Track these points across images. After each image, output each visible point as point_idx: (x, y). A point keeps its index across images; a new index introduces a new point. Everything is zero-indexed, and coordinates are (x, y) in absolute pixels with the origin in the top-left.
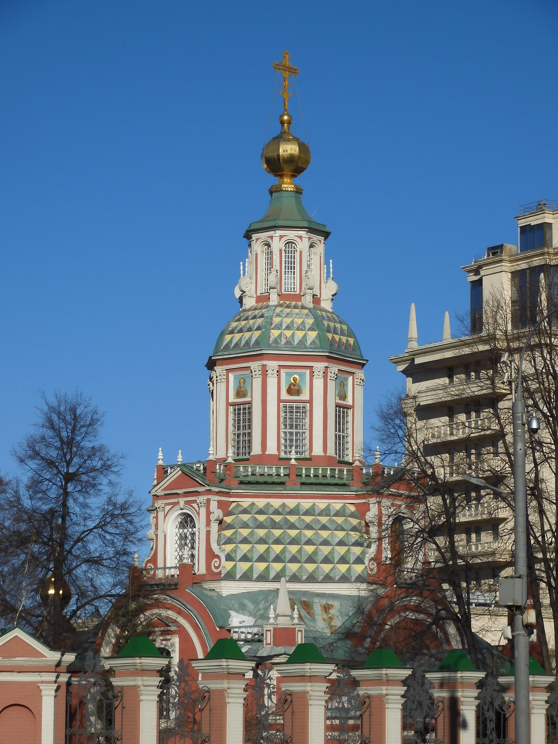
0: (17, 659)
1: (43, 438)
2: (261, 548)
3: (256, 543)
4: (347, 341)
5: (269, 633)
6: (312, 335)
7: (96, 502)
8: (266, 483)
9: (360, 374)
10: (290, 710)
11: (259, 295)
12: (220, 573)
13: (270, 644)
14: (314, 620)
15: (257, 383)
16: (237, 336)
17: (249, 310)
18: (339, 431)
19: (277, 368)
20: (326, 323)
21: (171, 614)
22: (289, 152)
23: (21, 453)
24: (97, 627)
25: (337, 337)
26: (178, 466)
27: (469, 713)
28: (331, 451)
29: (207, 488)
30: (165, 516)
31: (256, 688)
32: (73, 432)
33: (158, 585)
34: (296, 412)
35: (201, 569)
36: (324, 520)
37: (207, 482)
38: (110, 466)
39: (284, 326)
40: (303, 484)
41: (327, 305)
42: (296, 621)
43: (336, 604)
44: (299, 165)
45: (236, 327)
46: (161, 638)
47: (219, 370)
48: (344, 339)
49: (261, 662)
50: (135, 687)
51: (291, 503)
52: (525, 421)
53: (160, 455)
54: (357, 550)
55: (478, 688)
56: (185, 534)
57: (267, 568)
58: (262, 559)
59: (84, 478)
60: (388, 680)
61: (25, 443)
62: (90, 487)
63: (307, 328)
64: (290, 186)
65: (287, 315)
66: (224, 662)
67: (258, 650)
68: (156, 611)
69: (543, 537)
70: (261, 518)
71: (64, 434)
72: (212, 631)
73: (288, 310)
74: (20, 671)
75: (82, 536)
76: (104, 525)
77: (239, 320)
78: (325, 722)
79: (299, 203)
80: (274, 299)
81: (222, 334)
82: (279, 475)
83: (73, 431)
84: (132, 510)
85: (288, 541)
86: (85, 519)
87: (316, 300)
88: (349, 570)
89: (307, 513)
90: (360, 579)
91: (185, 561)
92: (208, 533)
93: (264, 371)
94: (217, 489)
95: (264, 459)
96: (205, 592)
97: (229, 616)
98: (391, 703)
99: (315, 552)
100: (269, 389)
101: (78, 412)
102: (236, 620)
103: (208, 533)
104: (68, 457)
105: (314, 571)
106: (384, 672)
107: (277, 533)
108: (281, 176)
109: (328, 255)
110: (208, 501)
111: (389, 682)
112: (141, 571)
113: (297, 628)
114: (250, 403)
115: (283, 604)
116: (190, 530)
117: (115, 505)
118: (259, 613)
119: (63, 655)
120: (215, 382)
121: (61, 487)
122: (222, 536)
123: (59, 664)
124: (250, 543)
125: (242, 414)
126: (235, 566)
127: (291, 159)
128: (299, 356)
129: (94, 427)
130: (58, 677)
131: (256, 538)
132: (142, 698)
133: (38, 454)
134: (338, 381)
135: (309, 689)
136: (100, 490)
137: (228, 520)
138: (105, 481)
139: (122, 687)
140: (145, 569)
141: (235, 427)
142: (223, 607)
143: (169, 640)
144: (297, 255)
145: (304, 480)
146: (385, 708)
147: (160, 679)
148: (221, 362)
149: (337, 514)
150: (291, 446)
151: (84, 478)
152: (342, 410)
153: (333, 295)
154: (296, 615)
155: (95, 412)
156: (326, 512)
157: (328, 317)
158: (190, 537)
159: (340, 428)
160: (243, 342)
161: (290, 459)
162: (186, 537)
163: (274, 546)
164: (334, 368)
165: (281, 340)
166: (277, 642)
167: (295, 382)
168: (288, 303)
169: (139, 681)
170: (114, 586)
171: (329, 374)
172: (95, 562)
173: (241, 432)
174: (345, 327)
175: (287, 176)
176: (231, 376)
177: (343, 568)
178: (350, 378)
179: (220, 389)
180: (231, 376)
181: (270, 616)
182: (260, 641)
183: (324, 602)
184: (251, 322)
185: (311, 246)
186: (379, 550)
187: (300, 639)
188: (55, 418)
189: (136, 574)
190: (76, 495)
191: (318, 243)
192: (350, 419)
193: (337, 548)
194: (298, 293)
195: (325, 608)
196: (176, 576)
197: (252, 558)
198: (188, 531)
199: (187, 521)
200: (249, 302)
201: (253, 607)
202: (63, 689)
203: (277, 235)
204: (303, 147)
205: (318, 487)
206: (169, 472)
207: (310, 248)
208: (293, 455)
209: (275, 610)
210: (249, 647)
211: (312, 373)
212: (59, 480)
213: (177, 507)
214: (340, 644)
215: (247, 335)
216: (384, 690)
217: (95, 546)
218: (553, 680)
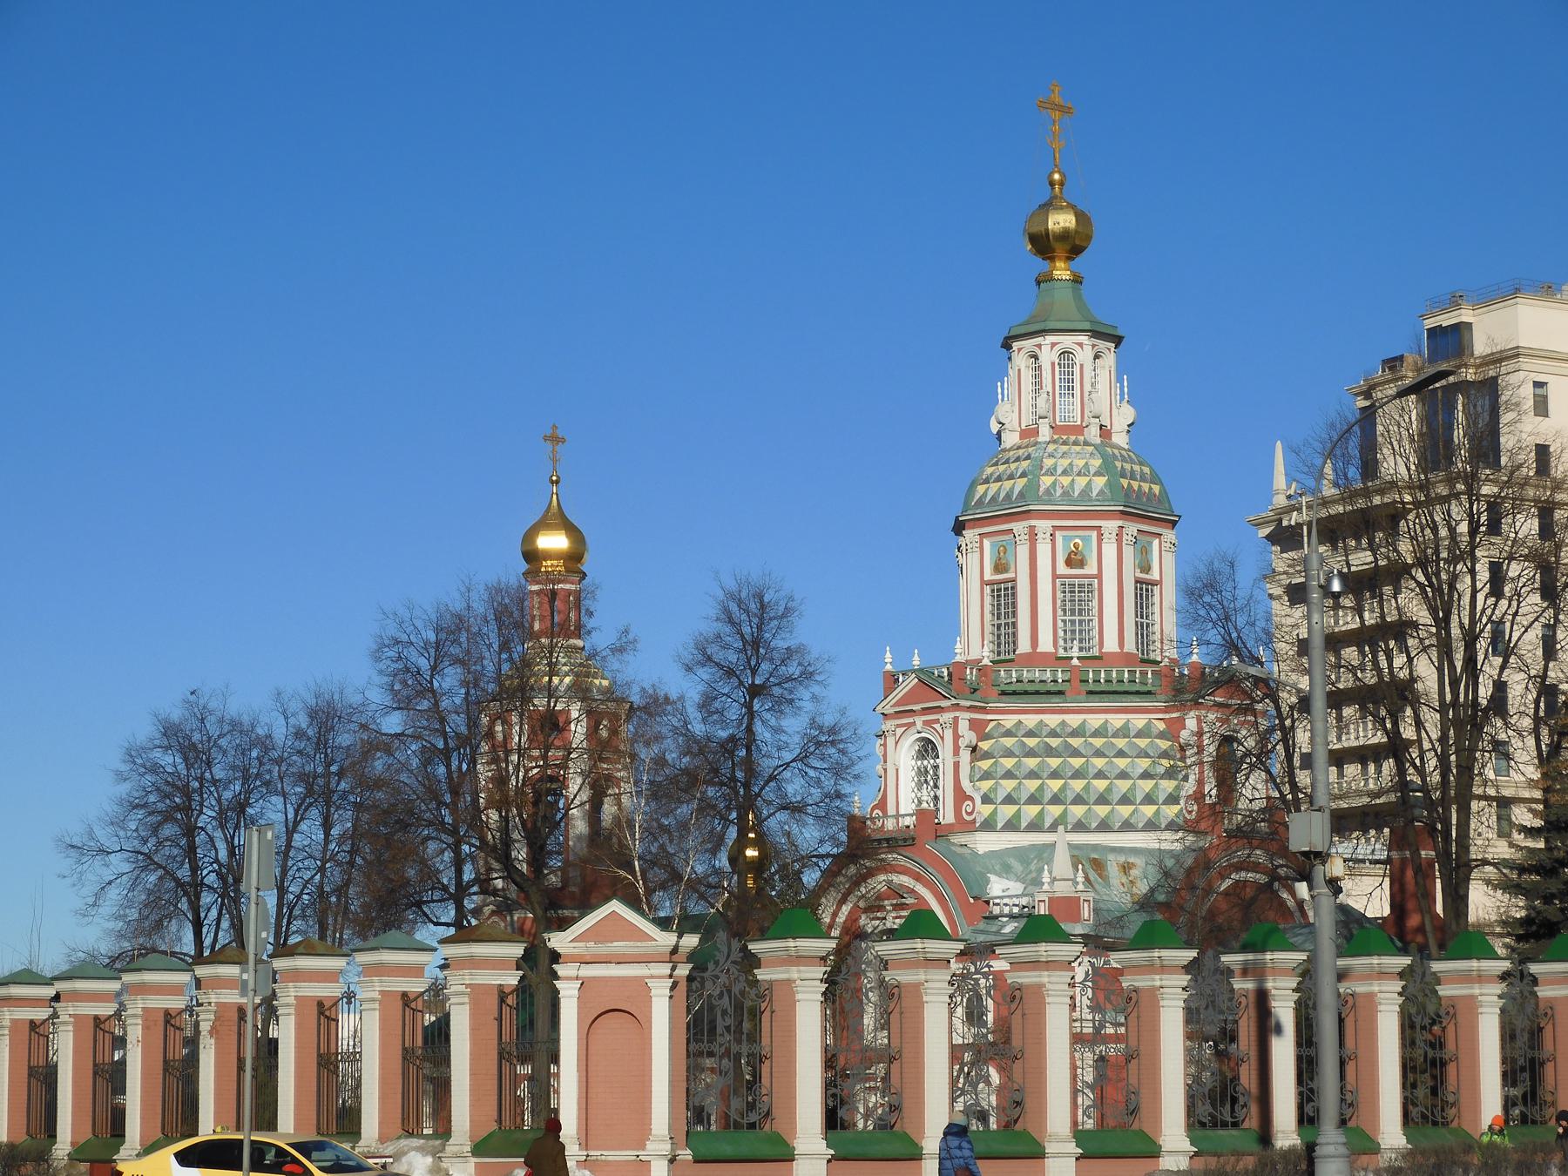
2: (1032, 785)
6: (1100, 482)
7: (794, 726)
8: (1037, 693)
9: (1169, 535)
10: (1019, 1012)
14: (1107, 884)
15: (1023, 552)
16: (994, 487)
19: (1050, 531)
20: (1119, 464)
21: (905, 880)
23: (688, 658)
25: (1135, 485)
26: (914, 671)
27: (1284, 1011)
28: (1130, 646)
29: (954, 701)
32: (759, 628)
33: (887, 840)
35: (947, 816)
36: (1121, 743)
38: (811, 674)
39: (1059, 471)
40: (1090, 693)
41: (1120, 439)
42: (1081, 887)
43: (1139, 861)
48: (1145, 487)
50: (789, 982)
51: (1074, 720)
53: (888, 657)
54: (1168, 786)
55: (1187, 973)
58: (1033, 800)
59: (777, 691)
62: (783, 704)
65: (1064, 455)
66: (918, 944)
68: (882, 877)
69: (1422, 759)
70: (1031, 742)
71: (746, 630)
73: (1065, 448)
74: (621, 961)
77: (996, 464)
79: (1078, 297)
80: (1045, 433)
83: (759, 628)
84: (844, 735)
86: (779, 749)
87: (1105, 432)
88: (1157, 812)
90: (1172, 826)
91: (925, 805)
92: (957, 765)
93: (1033, 535)
94: (968, 703)
95: (1034, 659)
97: (988, 881)
99: (1109, 789)
100: (1040, 559)
101: (766, 599)
102: (997, 887)
103: (957, 765)
104: (753, 663)
107: (1054, 762)
108: (1052, 259)
109: (1120, 371)
110: (956, 719)
111: (1164, 969)
113: (1083, 896)
114: (1014, 580)
115: (1061, 862)
117: (820, 728)
119: (680, 937)
123: (675, 950)
125: (1003, 595)
127: (1065, 235)
128: (1081, 512)
130: (673, 969)
131: (1024, 771)
132: (798, 996)
133: (709, 659)
135: (1046, 980)
136: (799, 708)
137: (985, 746)
138: (806, 695)
139: (771, 982)
140: (872, 819)
145: (1091, 687)
149: (1139, 734)
150: (1072, 640)
151: (777, 691)
152: (1145, 588)
154: (1080, 879)
155: (791, 599)
156: (1123, 732)
160: (1002, 495)
162: (927, 772)
163: (1095, 782)
164: (1132, 528)
169: (794, 973)
170: (821, 841)
173: (1003, 622)
176: (986, 543)
177: (1149, 811)
178: (1156, 542)
179: (971, 562)
183: (1122, 859)
185: (1097, 357)
186: (1200, 782)
188: (734, 607)
189: (856, 825)
190: (767, 716)
192: (1156, 599)
193: (1140, 782)
198: (928, 763)
199: (927, 748)
200: (1011, 439)
202: (683, 986)
204: (1081, 217)
208: (1075, 653)
209: (1050, 872)
212: (740, 694)
213: (913, 730)
214: (1134, 917)
215: (1008, 484)
217: (794, 787)
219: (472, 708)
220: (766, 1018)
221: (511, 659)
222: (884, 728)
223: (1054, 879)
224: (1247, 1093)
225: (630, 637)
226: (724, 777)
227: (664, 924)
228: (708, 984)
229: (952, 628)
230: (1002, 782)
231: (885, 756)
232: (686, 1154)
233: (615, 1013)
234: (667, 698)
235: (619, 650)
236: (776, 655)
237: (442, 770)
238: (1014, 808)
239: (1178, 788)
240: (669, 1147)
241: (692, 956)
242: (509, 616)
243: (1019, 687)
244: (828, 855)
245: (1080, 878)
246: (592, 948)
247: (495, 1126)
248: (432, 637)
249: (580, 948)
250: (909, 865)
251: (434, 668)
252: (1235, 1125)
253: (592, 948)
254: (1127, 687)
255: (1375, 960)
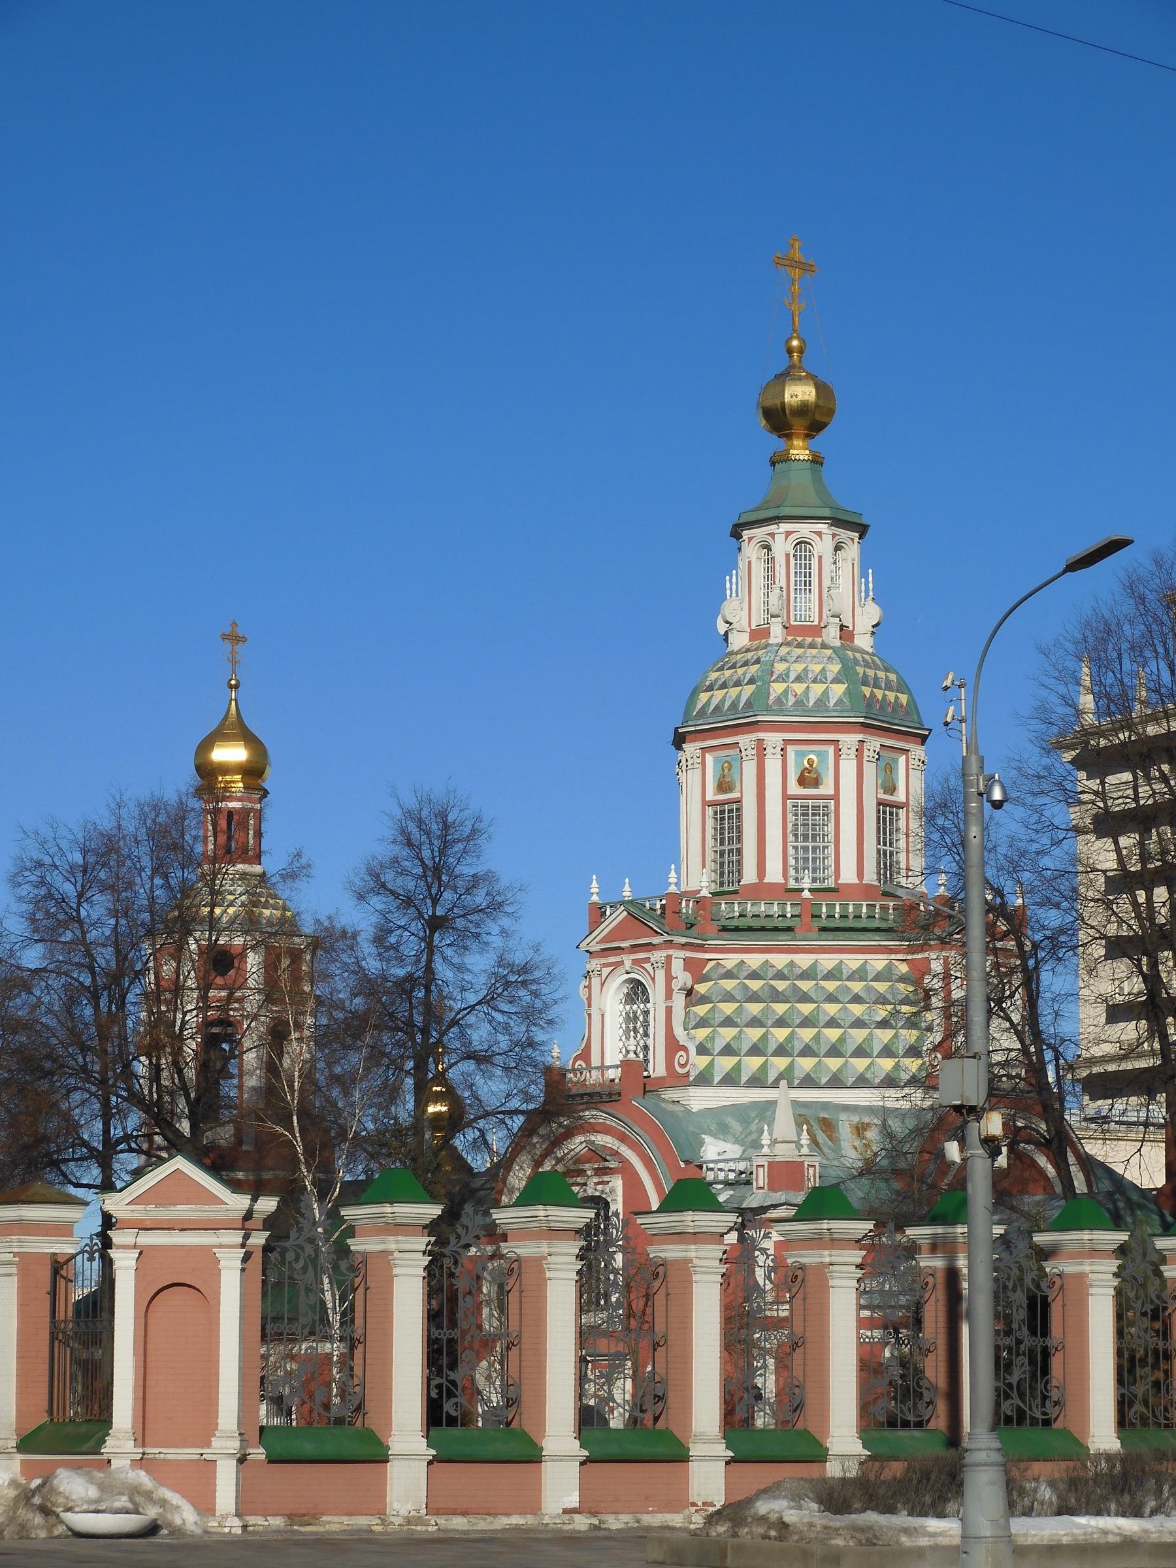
0: (179, 1207)
1: (395, 861)
2: (755, 1034)
3: (747, 1026)
4: (897, 698)
5: (761, 1169)
6: (839, 690)
7: (479, 964)
8: (763, 929)
11: (753, 627)
12: (688, 1074)
13: (763, 1188)
14: (837, 1149)
16: (718, 695)
17: (737, 653)
18: (885, 844)
19: (780, 745)
20: (860, 670)
22: (800, 397)
24: (496, 1167)
25: (879, 694)
26: (623, 903)
28: (870, 877)
30: (602, 985)
31: (739, 1261)
32: (442, 852)
33: (590, 1095)
34: (813, 815)
36: (857, 987)
37: (667, 929)
38: (500, 904)
39: (792, 676)
40: (823, 929)
41: (864, 641)
42: (805, 1150)
44: (818, 417)
45: (716, 680)
46: (596, 1180)
47: (690, 748)
48: (891, 696)
49: (749, 1218)
50: (386, 1254)
51: (804, 961)
52: (981, 788)
56: (635, 1013)
57: (764, 1066)
58: (755, 1051)
59: (460, 923)
60: (832, 1240)
61: (364, 870)
62: (468, 938)
63: (829, 679)
64: (802, 452)
65: (798, 659)
66: (540, 1211)
67: (743, 1198)
70: (755, 985)
71: (426, 854)
72: (671, 1164)
73: (800, 651)
75: (459, 1016)
76: (493, 999)
77: (721, 669)
78: (858, 1315)
79: (817, 480)
80: (777, 634)
81: (695, 693)
82: (785, 916)
83: (442, 852)
84: (537, 974)
85: (798, 1021)
86: (463, 989)
87: (846, 633)
88: (897, 1067)
89: (829, 976)
91: (632, 1056)
92: (669, 1011)
93: (761, 750)
94: (683, 940)
95: (761, 890)
96: (663, 1105)
97: (702, 1143)
98: (402, 1266)
99: (842, 1040)
100: (769, 777)
101: (450, 819)
103: (669, 1011)
104: (434, 891)
105: (840, 1070)
106: (825, 1226)
107: (780, 1008)
108: (789, 437)
109: (865, 563)
110: (669, 958)
111: (835, 1243)
112: (563, 1073)
114: (739, 801)
116: (642, 1006)
118: (750, 1138)
120: (684, 768)
121: (423, 939)
122: (691, 1016)
123: (248, 1215)
124: (735, 1025)
125: (727, 817)
126: (712, 1063)
127: (803, 410)
128: (816, 724)
129: (477, 842)
130: (246, 1237)
131: (746, 1018)
132: (396, 1271)
133: (383, 885)
134: (882, 764)
135: (692, 1254)
136: (487, 944)
137: (702, 988)
138: (495, 929)
139: (365, 1255)
140: (573, 1070)
141: (716, 839)
142: (692, 1129)
143: (608, 1182)
144: (815, 562)
145: (824, 923)
146: (828, 1288)
147: (427, 1239)
148: (693, 736)
149: (878, 977)
151: (460, 923)
153: (873, 626)
155: (479, 819)
156: (859, 974)
157: (864, 660)
158: (641, 1018)
159: (885, 839)
161: (802, 890)
162: (636, 1018)
164: (874, 743)
165: (787, 699)
166: (773, 1185)
167: (811, 766)
168: (799, 639)
169: (391, 1243)
170: (509, 1095)
171: (866, 753)
172: (482, 1059)
173: (726, 848)
174: (893, 677)
175: (798, 437)
176: (709, 758)
179: (690, 780)
180: (709, 758)
181: (763, 1142)
182: (748, 1183)
184: (740, 671)
185: (838, 548)
187: (812, 1179)
188: (412, 828)
189: (554, 1078)
190: (449, 952)
191: (849, 542)
193: (878, 1031)
194: (816, 623)
195: (857, 1128)
196: (617, 1081)
197: (740, 1050)
198: (638, 1007)
199: (637, 991)
200: (739, 641)
201: (740, 1129)
202: (257, 1258)
203: (781, 530)
205: (847, 934)
206: (608, 913)
207: (836, 550)
208: (807, 883)
209: (771, 1134)
210: (731, 1192)
211: (838, 751)
213: (621, 970)
215: (733, 692)
216: (826, 1256)
217: (480, 1035)
218: (1126, 1238)
219: (122, 945)
220: (659, 1299)
221: (167, 886)
222: (588, 967)
223: (775, 1142)
224: (933, 1388)
225: (303, 861)
226: (405, 1022)
227: (236, 1186)
228: (290, 1256)
229: (671, 853)
230: (720, 1029)
231: (589, 999)
232: (258, 1453)
233: (178, 1288)
234: (344, 932)
235: (290, 876)
236: (460, 883)
237: (88, 1011)
238: (732, 1061)
239: (920, 1039)
240: (237, 1444)
241: (270, 1223)
242: (166, 837)
243: (741, 923)
244: (517, 1112)
245: (805, 1140)
246: (152, 1212)
247: (45, 1418)
248: (78, 858)
249: (138, 1212)
250: (613, 1122)
251: (80, 896)
252: (919, 1425)
253: (152, 1212)
254: (851, 923)
255: (1086, 1236)
